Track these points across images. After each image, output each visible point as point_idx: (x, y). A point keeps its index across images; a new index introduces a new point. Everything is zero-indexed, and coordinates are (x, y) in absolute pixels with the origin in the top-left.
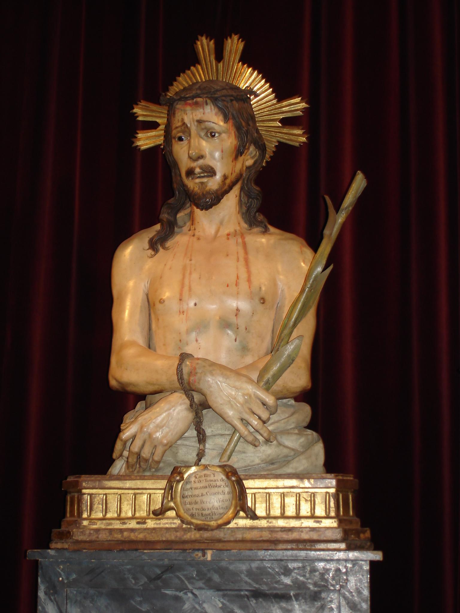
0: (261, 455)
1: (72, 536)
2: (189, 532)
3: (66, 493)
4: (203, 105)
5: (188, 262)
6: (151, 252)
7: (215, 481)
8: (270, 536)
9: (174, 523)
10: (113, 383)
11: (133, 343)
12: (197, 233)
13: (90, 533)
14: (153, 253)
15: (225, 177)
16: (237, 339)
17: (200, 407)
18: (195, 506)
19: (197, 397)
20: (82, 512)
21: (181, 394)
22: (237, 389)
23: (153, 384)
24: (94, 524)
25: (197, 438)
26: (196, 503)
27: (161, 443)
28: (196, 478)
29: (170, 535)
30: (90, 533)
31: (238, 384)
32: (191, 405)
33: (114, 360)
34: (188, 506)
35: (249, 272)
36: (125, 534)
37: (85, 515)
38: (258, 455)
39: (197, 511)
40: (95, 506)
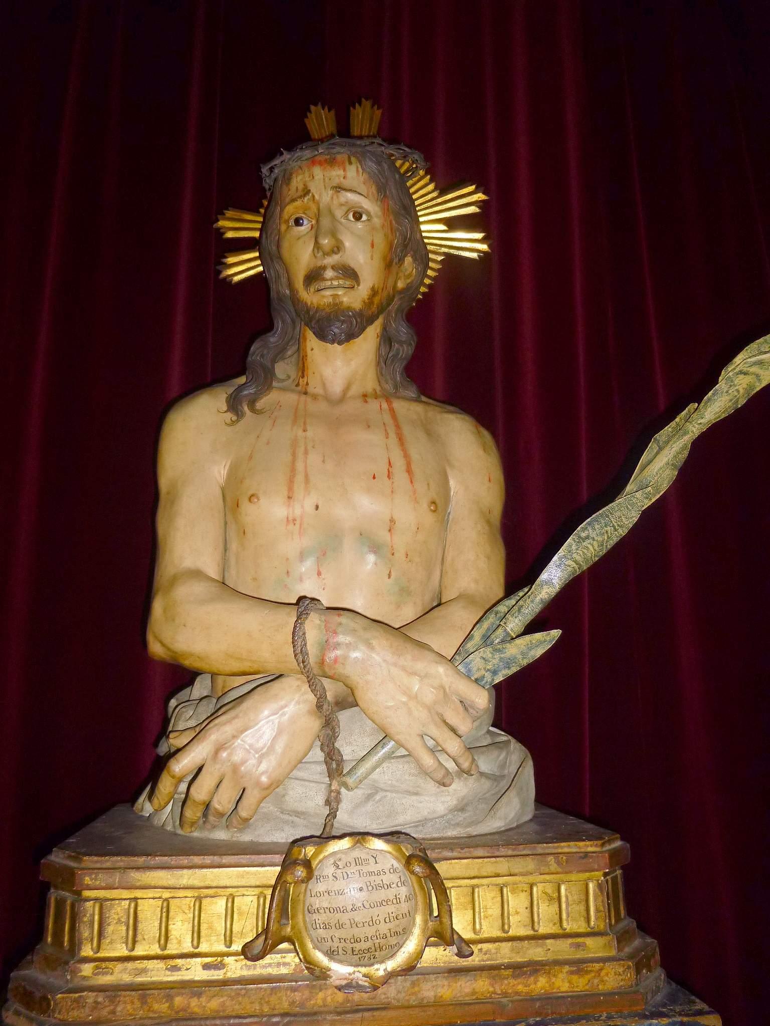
0: (449, 798)
1: (54, 1011)
2: (321, 990)
3: (46, 887)
4: (343, 163)
5: (300, 433)
6: (229, 416)
7: (379, 874)
8: (491, 989)
9: (285, 964)
10: (156, 649)
11: (197, 574)
12: (310, 389)
13: (96, 1002)
14: (234, 418)
15: (374, 292)
16: (393, 574)
17: (336, 704)
18: (338, 934)
19: (331, 689)
20: (81, 943)
21: (299, 683)
22: (424, 677)
23: (240, 659)
24: (106, 973)
25: (324, 767)
26: (341, 926)
27: (258, 783)
28: (338, 867)
29: (280, 999)
30: (96, 1002)
31: (420, 666)
32: (319, 707)
33: (158, 607)
34: (321, 932)
35: (406, 456)
36: (178, 1001)
37: (87, 951)
38: (443, 799)
39: (343, 944)
40: (110, 929)
